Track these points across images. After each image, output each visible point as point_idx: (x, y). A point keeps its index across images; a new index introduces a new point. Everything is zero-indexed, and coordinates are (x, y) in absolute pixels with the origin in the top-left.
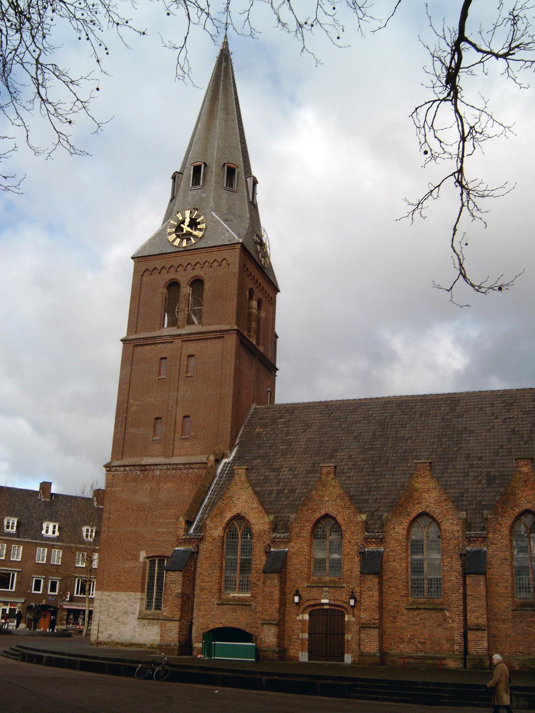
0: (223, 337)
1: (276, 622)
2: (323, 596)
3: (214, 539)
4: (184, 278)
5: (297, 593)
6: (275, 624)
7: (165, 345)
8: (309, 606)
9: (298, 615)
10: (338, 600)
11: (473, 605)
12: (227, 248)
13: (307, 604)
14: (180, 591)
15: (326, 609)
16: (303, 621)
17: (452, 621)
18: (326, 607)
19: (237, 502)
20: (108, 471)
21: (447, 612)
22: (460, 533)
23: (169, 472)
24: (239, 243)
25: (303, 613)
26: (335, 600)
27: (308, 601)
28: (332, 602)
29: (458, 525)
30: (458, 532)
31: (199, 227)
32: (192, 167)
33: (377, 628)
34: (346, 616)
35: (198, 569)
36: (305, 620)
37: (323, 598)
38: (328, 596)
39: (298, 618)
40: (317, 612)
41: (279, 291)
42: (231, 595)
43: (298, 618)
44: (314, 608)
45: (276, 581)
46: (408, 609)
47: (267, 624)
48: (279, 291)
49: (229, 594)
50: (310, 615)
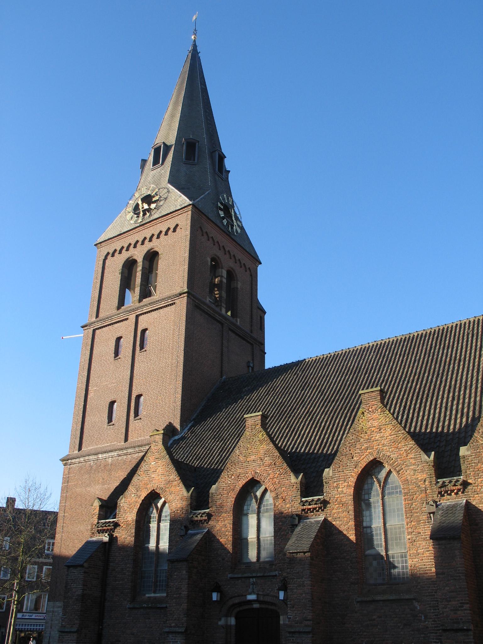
0: (174, 303)
1: (183, 630)
2: (250, 590)
3: (128, 525)
4: (139, 254)
5: (217, 589)
6: (181, 632)
7: (121, 323)
8: (234, 605)
9: (220, 619)
10: (268, 595)
11: (447, 588)
12: (179, 212)
13: (230, 603)
14: (80, 592)
15: (256, 609)
16: (227, 627)
17: (426, 617)
18: (256, 606)
19: (153, 476)
20: (65, 465)
21: (416, 604)
22: (427, 483)
23: (120, 458)
24: (190, 205)
25: (227, 615)
26: (264, 595)
27: (231, 598)
28: (261, 598)
29: (422, 471)
30: (425, 481)
31: (154, 199)
32: (153, 150)
33: (308, 633)
34: (281, 617)
35: (111, 564)
36: (231, 626)
37: (250, 594)
38: (255, 591)
39: (220, 623)
40: (244, 613)
41: (261, 263)
42: (147, 595)
43: (220, 623)
44: (241, 609)
45: (184, 572)
46: (361, 602)
47: (172, 632)
48: (261, 263)
49: (145, 595)
50: (237, 618)
